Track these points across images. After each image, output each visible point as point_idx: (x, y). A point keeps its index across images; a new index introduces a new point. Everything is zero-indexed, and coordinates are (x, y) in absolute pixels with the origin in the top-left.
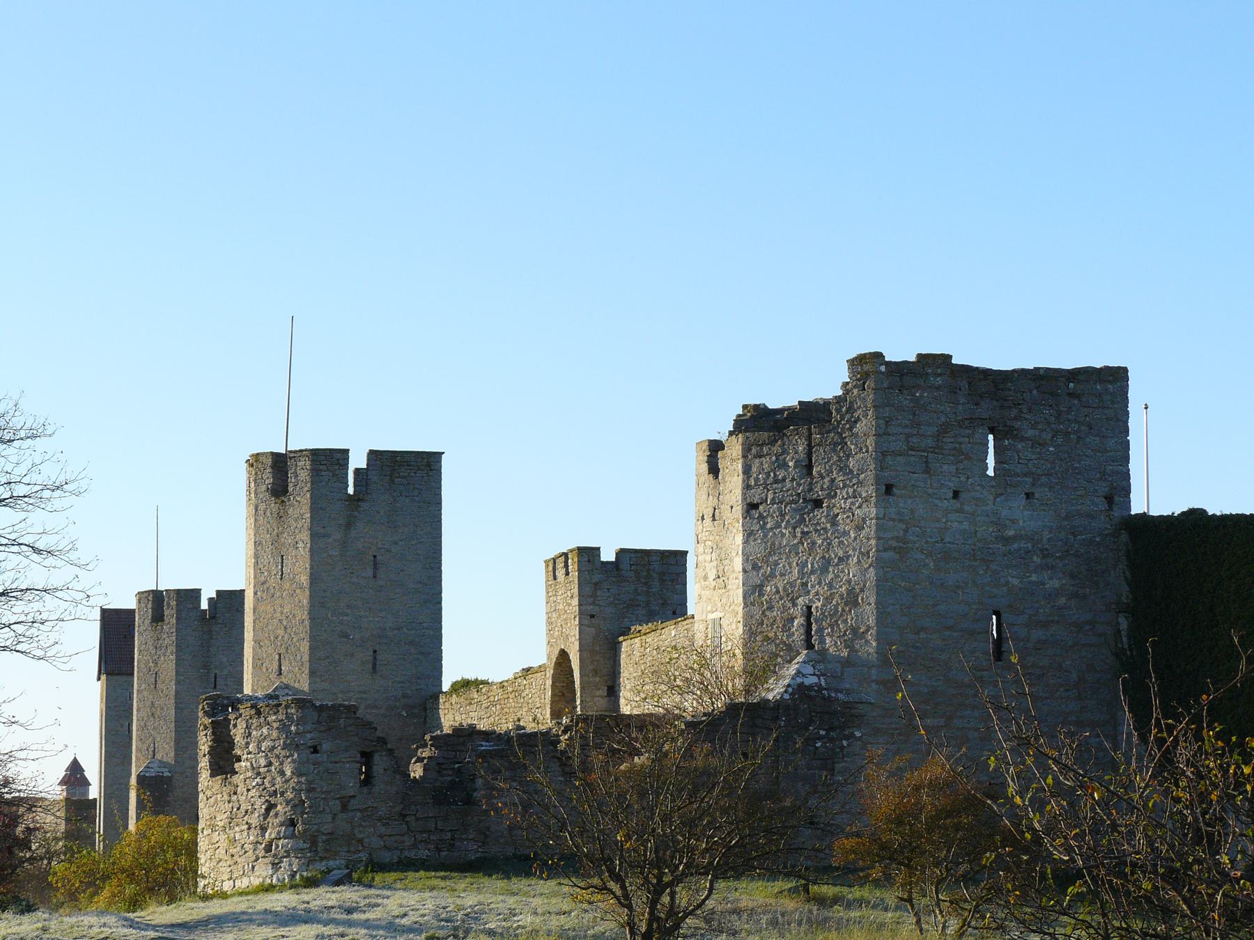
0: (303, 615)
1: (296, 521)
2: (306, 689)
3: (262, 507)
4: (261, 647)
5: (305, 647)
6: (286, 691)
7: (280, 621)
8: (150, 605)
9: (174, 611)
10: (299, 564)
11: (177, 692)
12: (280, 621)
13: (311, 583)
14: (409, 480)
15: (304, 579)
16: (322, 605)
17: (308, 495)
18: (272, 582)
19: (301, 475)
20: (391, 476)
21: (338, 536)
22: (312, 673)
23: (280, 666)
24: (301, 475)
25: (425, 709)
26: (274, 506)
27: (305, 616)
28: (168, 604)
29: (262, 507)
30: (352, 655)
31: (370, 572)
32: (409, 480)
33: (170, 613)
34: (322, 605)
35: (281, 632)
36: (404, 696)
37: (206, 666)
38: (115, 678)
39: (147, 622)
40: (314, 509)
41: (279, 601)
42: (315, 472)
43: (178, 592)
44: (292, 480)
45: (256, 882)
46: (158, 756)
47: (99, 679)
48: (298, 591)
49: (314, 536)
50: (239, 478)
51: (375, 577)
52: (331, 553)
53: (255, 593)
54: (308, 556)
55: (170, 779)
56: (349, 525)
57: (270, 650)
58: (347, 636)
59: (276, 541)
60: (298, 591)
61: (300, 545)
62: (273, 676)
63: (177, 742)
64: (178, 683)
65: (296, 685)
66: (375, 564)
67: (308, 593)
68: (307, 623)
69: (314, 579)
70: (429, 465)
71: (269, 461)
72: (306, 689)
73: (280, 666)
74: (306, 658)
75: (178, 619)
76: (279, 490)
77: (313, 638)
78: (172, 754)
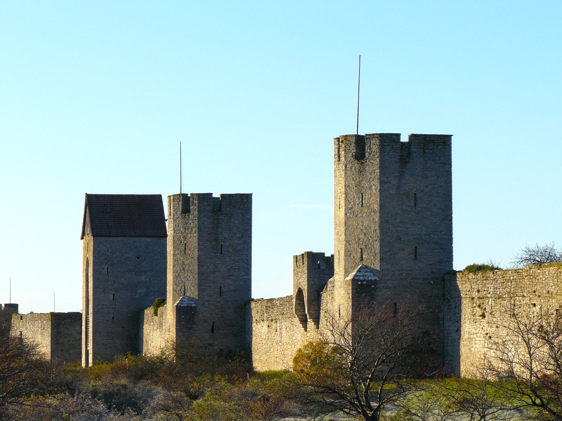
0: (376, 226)
1: (370, 174)
2: (378, 268)
3: (349, 166)
4: (350, 244)
5: (377, 245)
6: (366, 269)
7: (362, 230)
8: (181, 203)
9: (196, 207)
10: (373, 198)
11: (199, 256)
12: (362, 230)
13: (380, 209)
14: (433, 151)
15: (376, 207)
16: (387, 221)
17: (378, 160)
18: (356, 208)
19: (374, 148)
20: (424, 148)
21: (395, 182)
22: (382, 260)
23: (362, 255)
24: (374, 148)
25: (444, 280)
26: (356, 165)
27: (377, 228)
28: (193, 203)
29: (349, 166)
30: (403, 250)
31: (412, 203)
32: (433, 151)
33: (194, 209)
34: (387, 221)
35: (362, 236)
36: (433, 272)
37: (216, 240)
38: (99, 238)
39: (179, 213)
40: (382, 167)
41: (360, 219)
42: (382, 147)
43: (199, 195)
44: (367, 150)
45: (555, 410)
46: (188, 294)
47: (82, 238)
48: (372, 213)
49: (381, 183)
50: (331, 148)
51: (415, 205)
52: (391, 192)
53: (346, 214)
54: (378, 193)
55: (195, 308)
56: (401, 176)
57: (356, 246)
58: (400, 239)
59: (358, 185)
60: (372, 213)
61: (373, 187)
62: (358, 261)
63: (199, 285)
64: (199, 250)
65: (372, 266)
66: (416, 198)
67: (378, 214)
68: (378, 231)
69: (382, 207)
70: (444, 142)
71: (354, 140)
72: (378, 268)
73: (362, 255)
74: (378, 251)
75: (199, 211)
76: (360, 156)
77: (381, 240)
78: (196, 293)
